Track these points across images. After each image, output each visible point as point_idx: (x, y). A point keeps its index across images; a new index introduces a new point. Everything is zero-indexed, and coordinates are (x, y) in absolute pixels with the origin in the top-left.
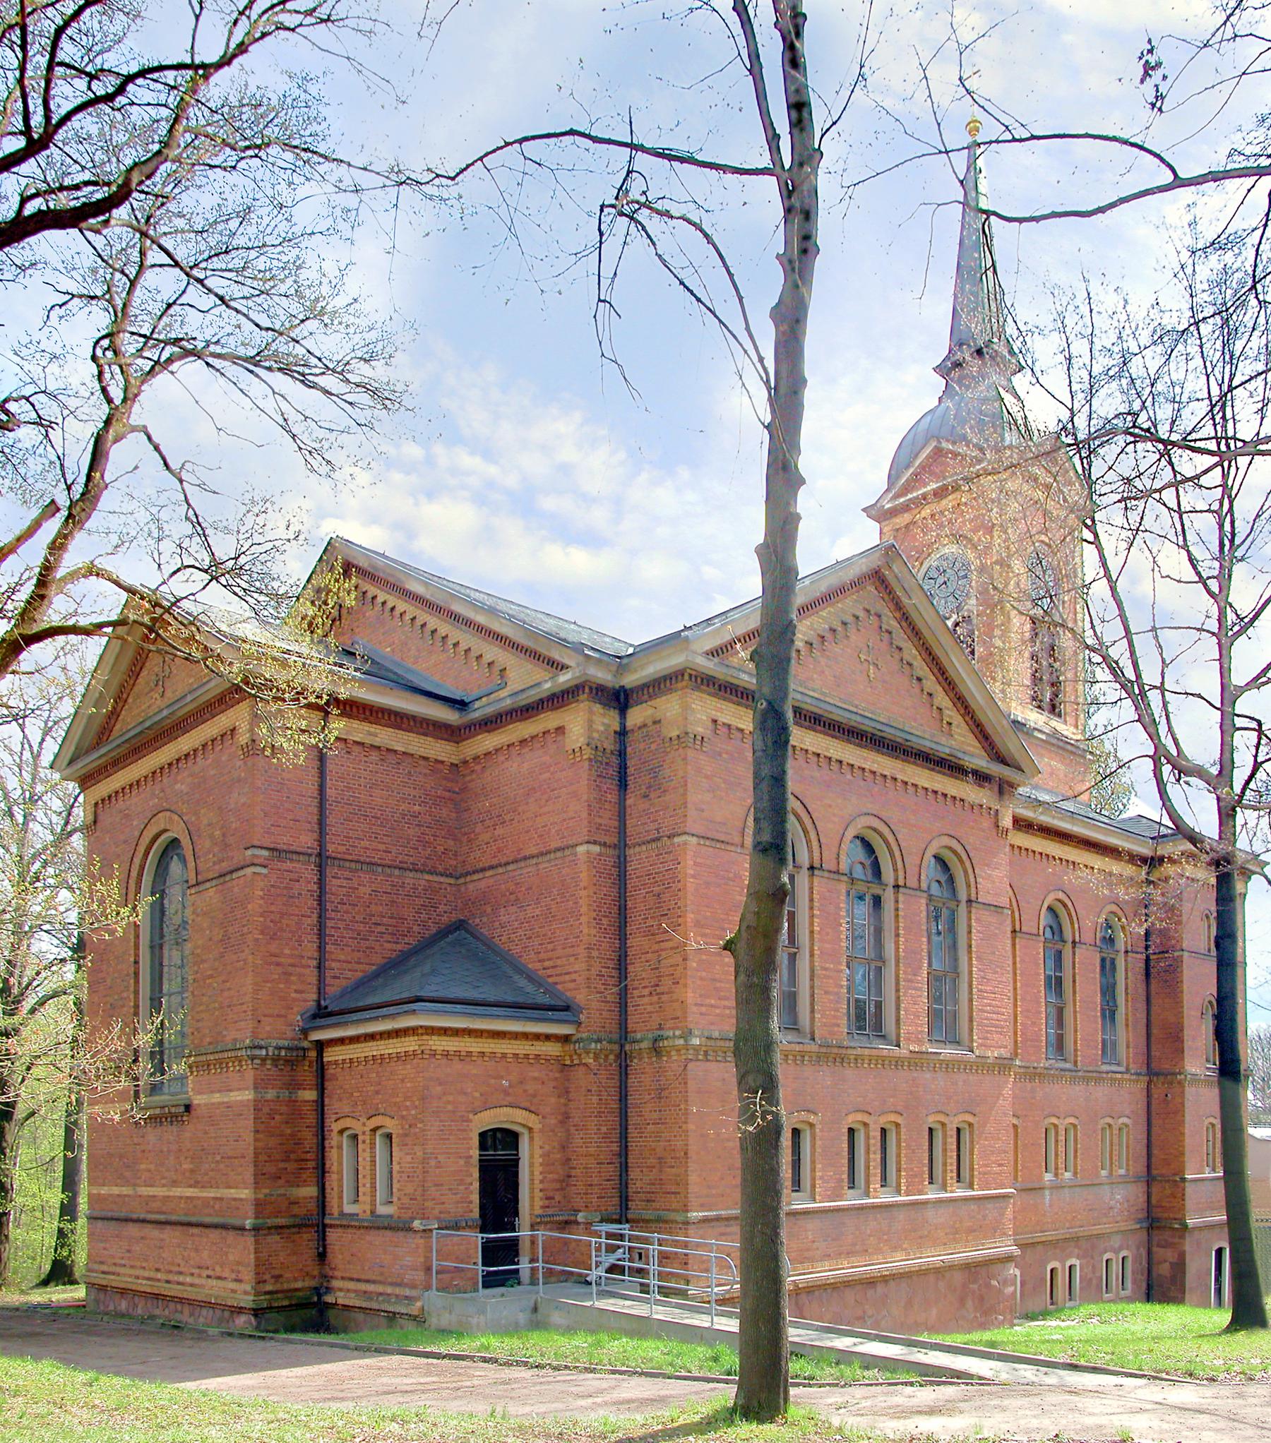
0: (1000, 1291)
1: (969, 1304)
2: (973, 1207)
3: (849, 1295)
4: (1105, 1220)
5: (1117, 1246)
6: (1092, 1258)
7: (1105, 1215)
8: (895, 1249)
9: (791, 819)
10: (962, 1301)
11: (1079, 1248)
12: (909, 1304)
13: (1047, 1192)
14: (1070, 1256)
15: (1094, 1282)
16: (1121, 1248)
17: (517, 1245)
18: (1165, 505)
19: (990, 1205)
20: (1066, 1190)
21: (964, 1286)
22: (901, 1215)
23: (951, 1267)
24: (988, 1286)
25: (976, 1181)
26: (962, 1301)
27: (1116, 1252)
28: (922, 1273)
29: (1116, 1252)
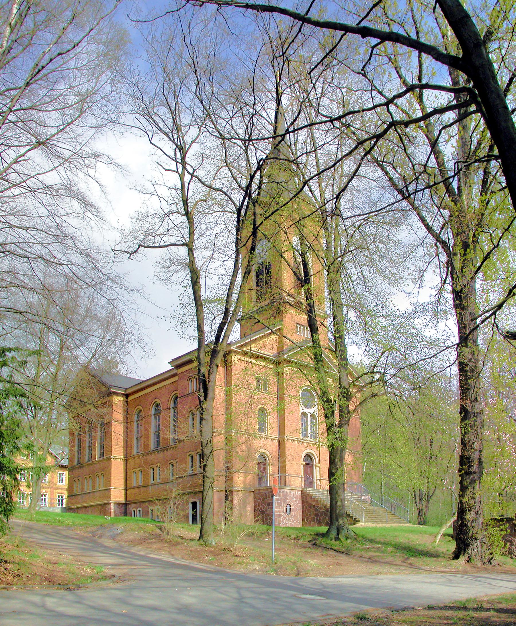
2: (103, 492)
13: (150, 487)
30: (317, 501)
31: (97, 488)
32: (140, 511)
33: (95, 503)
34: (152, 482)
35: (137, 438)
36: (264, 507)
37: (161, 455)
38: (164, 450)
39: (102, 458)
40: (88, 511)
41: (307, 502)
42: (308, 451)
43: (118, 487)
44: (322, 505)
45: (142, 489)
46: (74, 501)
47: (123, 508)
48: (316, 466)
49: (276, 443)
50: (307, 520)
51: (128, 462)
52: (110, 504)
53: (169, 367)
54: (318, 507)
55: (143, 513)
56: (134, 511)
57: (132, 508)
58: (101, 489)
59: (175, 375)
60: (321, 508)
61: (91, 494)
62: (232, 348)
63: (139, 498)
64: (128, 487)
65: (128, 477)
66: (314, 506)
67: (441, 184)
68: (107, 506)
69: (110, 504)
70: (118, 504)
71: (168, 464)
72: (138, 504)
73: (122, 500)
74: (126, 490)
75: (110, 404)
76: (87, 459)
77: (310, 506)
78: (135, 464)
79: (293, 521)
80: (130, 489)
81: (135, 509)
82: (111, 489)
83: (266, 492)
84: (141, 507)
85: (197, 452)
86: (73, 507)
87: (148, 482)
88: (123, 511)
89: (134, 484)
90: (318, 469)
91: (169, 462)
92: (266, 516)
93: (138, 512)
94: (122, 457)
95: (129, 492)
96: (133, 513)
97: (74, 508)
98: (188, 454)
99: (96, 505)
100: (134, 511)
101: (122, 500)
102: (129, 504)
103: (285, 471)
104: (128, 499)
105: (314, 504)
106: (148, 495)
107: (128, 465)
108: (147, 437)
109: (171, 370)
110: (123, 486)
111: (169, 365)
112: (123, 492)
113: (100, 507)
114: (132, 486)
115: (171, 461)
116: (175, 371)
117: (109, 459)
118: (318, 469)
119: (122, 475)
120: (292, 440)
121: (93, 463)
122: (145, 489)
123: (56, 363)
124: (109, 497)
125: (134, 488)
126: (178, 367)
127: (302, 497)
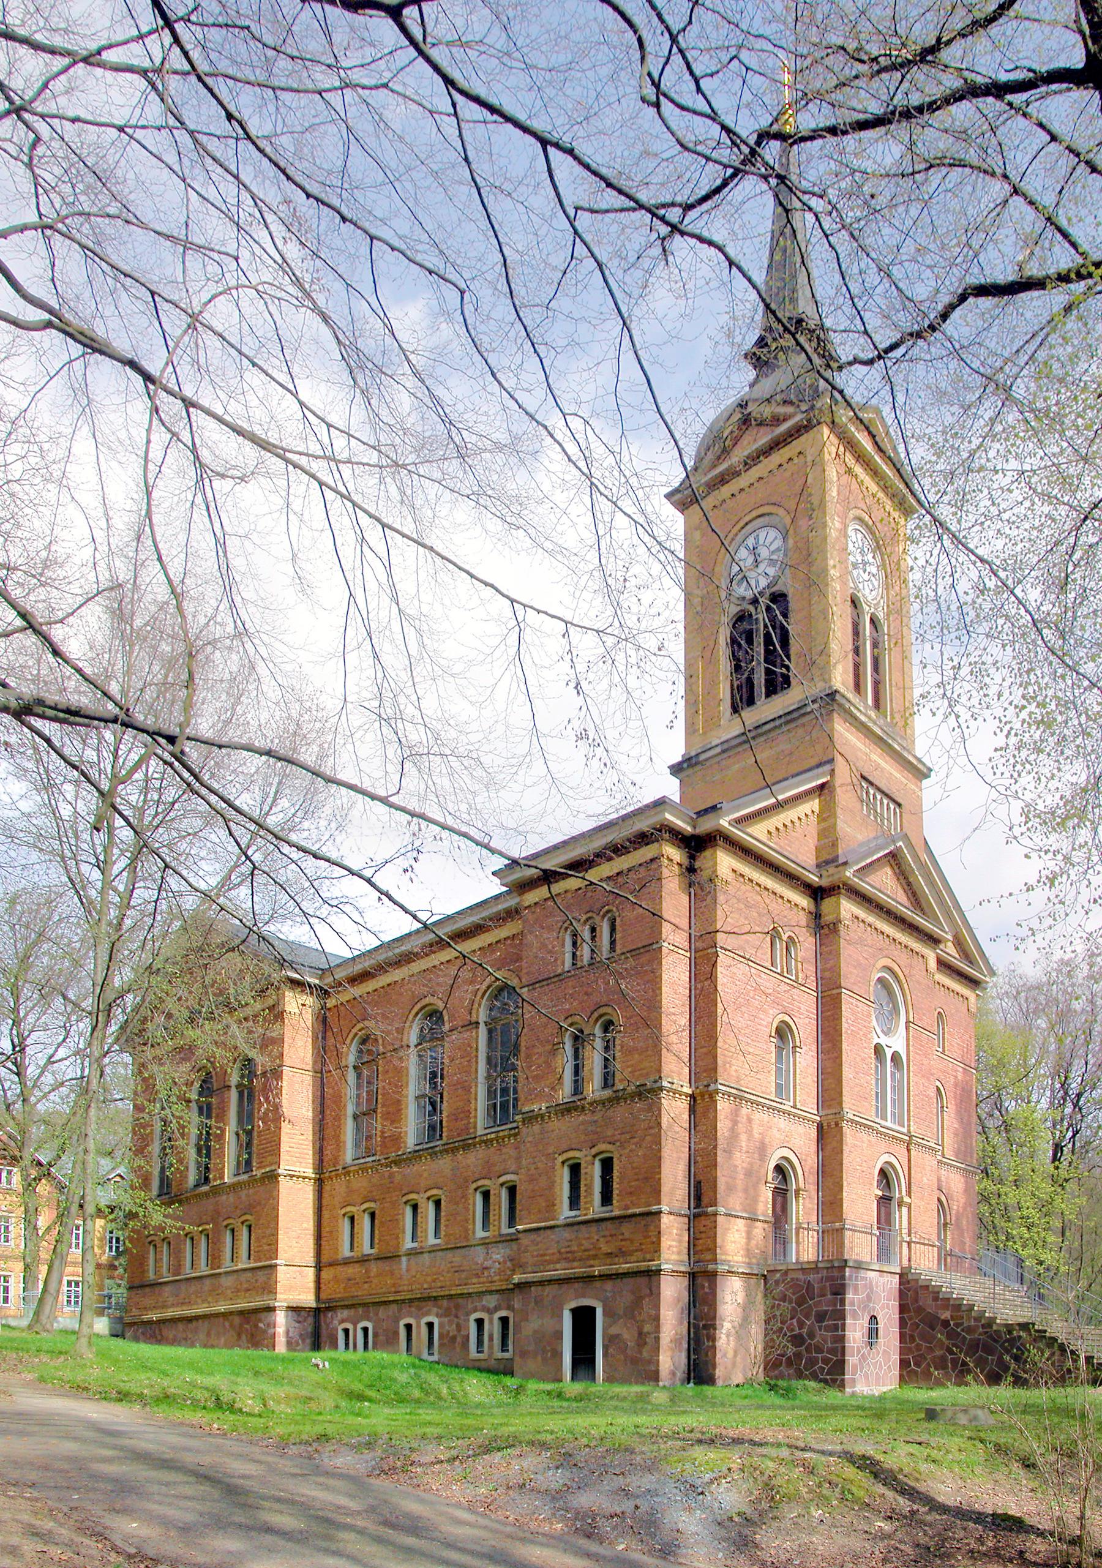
0: (265, 1332)
1: (244, 1337)
2: (249, 1274)
3: (181, 1326)
4: (475, 1280)
5: (492, 1305)
6: (457, 1316)
7: (477, 1276)
8: (203, 1301)
9: (907, 903)
10: (239, 1336)
11: (440, 1307)
12: (208, 1334)
13: (404, 1259)
14: (427, 1314)
15: (459, 1339)
16: (497, 1309)
17: (904, 1364)
18: (302, 404)
19: (260, 1273)
20: (426, 1255)
21: (241, 1325)
22: (208, 1282)
23: (231, 1313)
24: (256, 1326)
25: (643, 1265)
26: (239, 1336)
27: (491, 1312)
28: (217, 1315)
29: (491, 1312)
30: (957, 1307)
31: (188, 1271)
32: (430, 1325)
33: (221, 1308)
34: (408, 1244)
35: (355, 1117)
36: (801, 1325)
37: (445, 1164)
38: (454, 1150)
39: (245, 1177)
40: (196, 1331)
41: (920, 1310)
42: (886, 1158)
43: (297, 1262)
44: (976, 1319)
45: (374, 1268)
46: (148, 1302)
47: (310, 1320)
48: (900, 1204)
49: (813, 1133)
50: (917, 1364)
51: (327, 1187)
52: (273, 1309)
53: (495, 887)
54: (957, 1325)
55: (375, 1335)
56: (346, 1331)
57: (338, 1322)
58: (240, 1266)
59: (512, 914)
60: (969, 1330)
61: (208, 1282)
62: (722, 822)
63: (362, 1292)
64: (325, 1259)
65: (325, 1230)
66: (946, 1323)
67: (844, 353)
68: (263, 1315)
69: (273, 1309)
70: (295, 1310)
71: (471, 1191)
72: (360, 1310)
73: (308, 1299)
74: (319, 1267)
75: (277, 1014)
76: (192, 1178)
77: (932, 1322)
78: (350, 1191)
79: (881, 1367)
80: (330, 1265)
81: (350, 1326)
82: (276, 1266)
83: (811, 1277)
84: (369, 1320)
85: (594, 1151)
86: (145, 1318)
87: (398, 1246)
88: (310, 1329)
89: (346, 1252)
90: (904, 1210)
91: (474, 1186)
92: (808, 1350)
93: (424, 1330)
94: (310, 1172)
95: (326, 1274)
96: (341, 1336)
97: (150, 1322)
98: (561, 1159)
99: (225, 1315)
100: (346, 1331)
101: (308, 1299)
102: (328, 1309)
103: (840, 1218)
104: (323, 1296)
105: (946, 1315)
106: (394, 1285)
107: (325, 1195)
108: (395, 1114)
109: (497, 897)
110: (310, 1258)
111: (497, 880)
112: (311, 1273)
113: (237, 1320)
114: (340, 1257)
115: (480, 1183)
116: (512, 902)
117: (272, 1177)
118: (904, 1210)
119: (310, 1225)
120: (857, 1123)
121: (216, 1191)
122: (385, 1266)
123: (121, 888)
124: (270, 1288)
125: (347, 1262)
126: (523, 887)
127: (902, 1294)
